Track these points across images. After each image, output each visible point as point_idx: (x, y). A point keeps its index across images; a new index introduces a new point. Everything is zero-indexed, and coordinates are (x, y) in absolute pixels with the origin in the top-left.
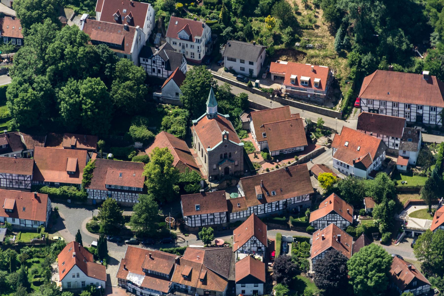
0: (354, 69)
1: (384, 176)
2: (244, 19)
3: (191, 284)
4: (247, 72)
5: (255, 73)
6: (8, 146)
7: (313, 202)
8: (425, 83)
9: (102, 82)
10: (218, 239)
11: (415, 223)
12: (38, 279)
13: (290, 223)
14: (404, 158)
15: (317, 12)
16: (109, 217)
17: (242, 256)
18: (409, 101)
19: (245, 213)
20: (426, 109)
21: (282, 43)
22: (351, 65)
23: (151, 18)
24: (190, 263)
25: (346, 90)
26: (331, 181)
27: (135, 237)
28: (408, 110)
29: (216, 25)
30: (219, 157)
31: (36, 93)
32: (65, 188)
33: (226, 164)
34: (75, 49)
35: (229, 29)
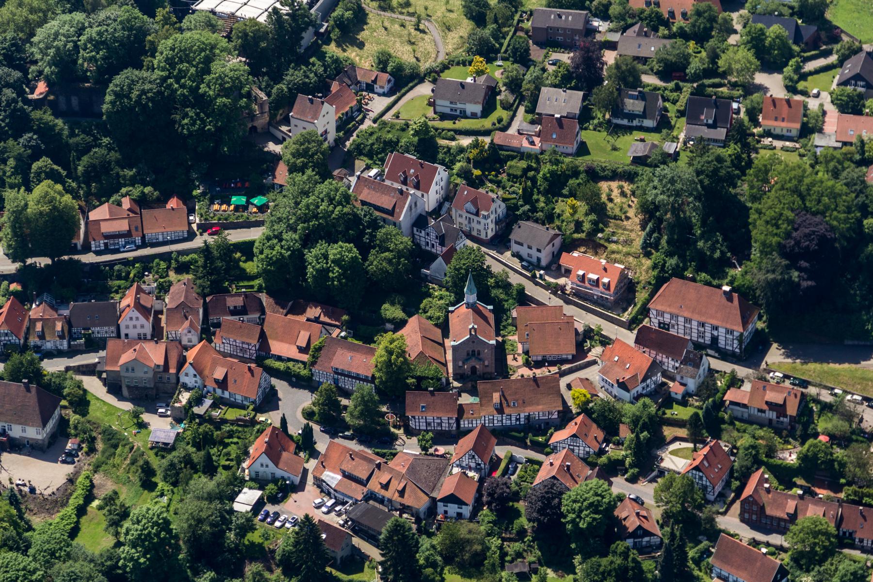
0: (655, 273)
1: (644, 402)
2: (547, 199)
3: (388, 494)
4: (534, 260)
5: (544, 263)
6: (244, 307)
7: (563, 420)
8: (724, 300)
9: (355, 249)
10: (439, 448)
11: (673, 462)
12: (227, 463)
13: (528, 441)
14: (682, 384)
15: (633, 201)
16: (323, 404)
17: (456, 470)
18: (703, 319)
19: (479, 422)
20: (722, 331)
21: (583, 232)
22: (655, 267)
23: (443, 184)
24: (391, 470)
25: (641, 296)
26: (583, 399)
27: (351, 432)
28: (701, 329)
29: (513, 201)
30: (470, 351)
31: (283, 251)
32: (290, 364)
33: (473, 362)
34: (331, 208)
35: (527, 207)
